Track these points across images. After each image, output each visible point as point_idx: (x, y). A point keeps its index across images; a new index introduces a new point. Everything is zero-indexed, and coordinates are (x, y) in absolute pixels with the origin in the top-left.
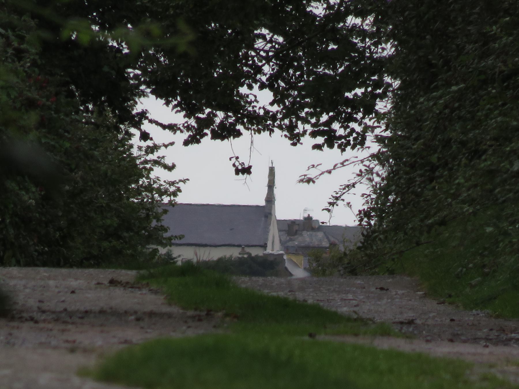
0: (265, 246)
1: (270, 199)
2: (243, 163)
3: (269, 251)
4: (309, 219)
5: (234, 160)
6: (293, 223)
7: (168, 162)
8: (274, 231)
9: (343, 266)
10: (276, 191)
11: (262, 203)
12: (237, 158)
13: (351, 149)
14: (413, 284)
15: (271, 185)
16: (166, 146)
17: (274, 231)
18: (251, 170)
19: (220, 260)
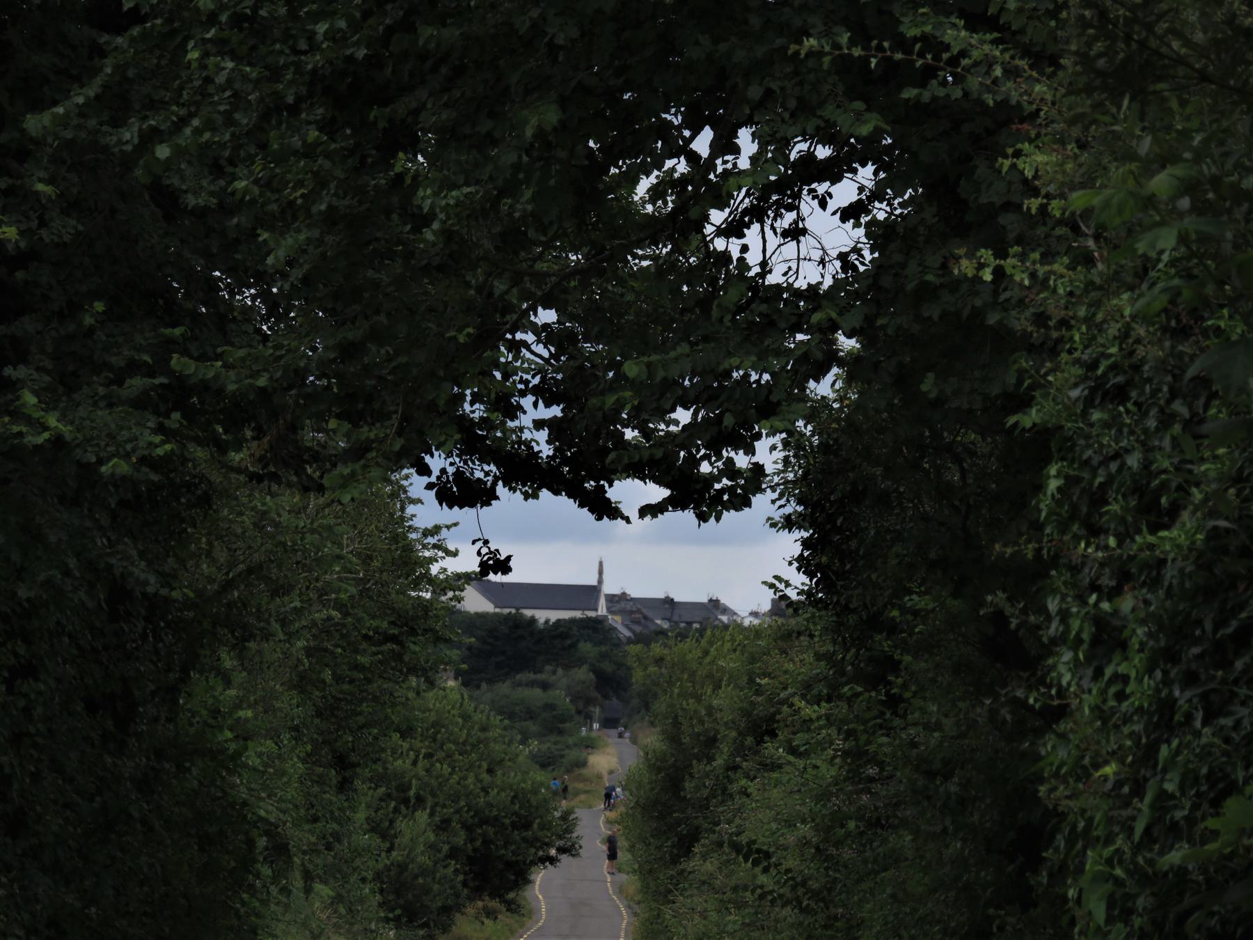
0: (596, 610)
1: (600, 581)
2: (497, 550)
3: (600, 613)
4: (624, 594)
5: (480, 544)
6: (614, 596)
7: (451, 547)
8: (602, 602)
9: (638, 629)
10: (604, 577)
11: (595, 583)
12: (486, 542)
13: (441, 505)
14: (513, 877)
15: (601, 573)
16: (448, 527)
17: (602, 602)
18: (512, 564)
19: (559, 621)
